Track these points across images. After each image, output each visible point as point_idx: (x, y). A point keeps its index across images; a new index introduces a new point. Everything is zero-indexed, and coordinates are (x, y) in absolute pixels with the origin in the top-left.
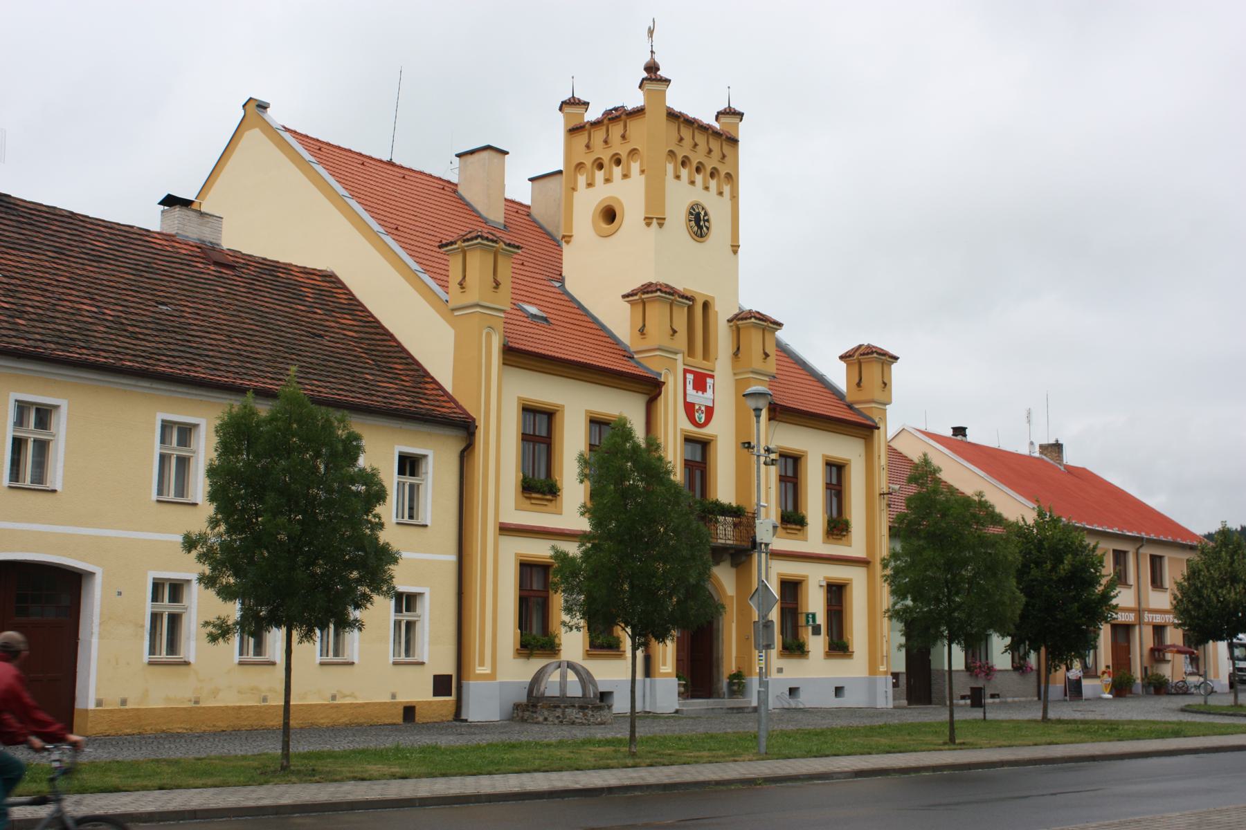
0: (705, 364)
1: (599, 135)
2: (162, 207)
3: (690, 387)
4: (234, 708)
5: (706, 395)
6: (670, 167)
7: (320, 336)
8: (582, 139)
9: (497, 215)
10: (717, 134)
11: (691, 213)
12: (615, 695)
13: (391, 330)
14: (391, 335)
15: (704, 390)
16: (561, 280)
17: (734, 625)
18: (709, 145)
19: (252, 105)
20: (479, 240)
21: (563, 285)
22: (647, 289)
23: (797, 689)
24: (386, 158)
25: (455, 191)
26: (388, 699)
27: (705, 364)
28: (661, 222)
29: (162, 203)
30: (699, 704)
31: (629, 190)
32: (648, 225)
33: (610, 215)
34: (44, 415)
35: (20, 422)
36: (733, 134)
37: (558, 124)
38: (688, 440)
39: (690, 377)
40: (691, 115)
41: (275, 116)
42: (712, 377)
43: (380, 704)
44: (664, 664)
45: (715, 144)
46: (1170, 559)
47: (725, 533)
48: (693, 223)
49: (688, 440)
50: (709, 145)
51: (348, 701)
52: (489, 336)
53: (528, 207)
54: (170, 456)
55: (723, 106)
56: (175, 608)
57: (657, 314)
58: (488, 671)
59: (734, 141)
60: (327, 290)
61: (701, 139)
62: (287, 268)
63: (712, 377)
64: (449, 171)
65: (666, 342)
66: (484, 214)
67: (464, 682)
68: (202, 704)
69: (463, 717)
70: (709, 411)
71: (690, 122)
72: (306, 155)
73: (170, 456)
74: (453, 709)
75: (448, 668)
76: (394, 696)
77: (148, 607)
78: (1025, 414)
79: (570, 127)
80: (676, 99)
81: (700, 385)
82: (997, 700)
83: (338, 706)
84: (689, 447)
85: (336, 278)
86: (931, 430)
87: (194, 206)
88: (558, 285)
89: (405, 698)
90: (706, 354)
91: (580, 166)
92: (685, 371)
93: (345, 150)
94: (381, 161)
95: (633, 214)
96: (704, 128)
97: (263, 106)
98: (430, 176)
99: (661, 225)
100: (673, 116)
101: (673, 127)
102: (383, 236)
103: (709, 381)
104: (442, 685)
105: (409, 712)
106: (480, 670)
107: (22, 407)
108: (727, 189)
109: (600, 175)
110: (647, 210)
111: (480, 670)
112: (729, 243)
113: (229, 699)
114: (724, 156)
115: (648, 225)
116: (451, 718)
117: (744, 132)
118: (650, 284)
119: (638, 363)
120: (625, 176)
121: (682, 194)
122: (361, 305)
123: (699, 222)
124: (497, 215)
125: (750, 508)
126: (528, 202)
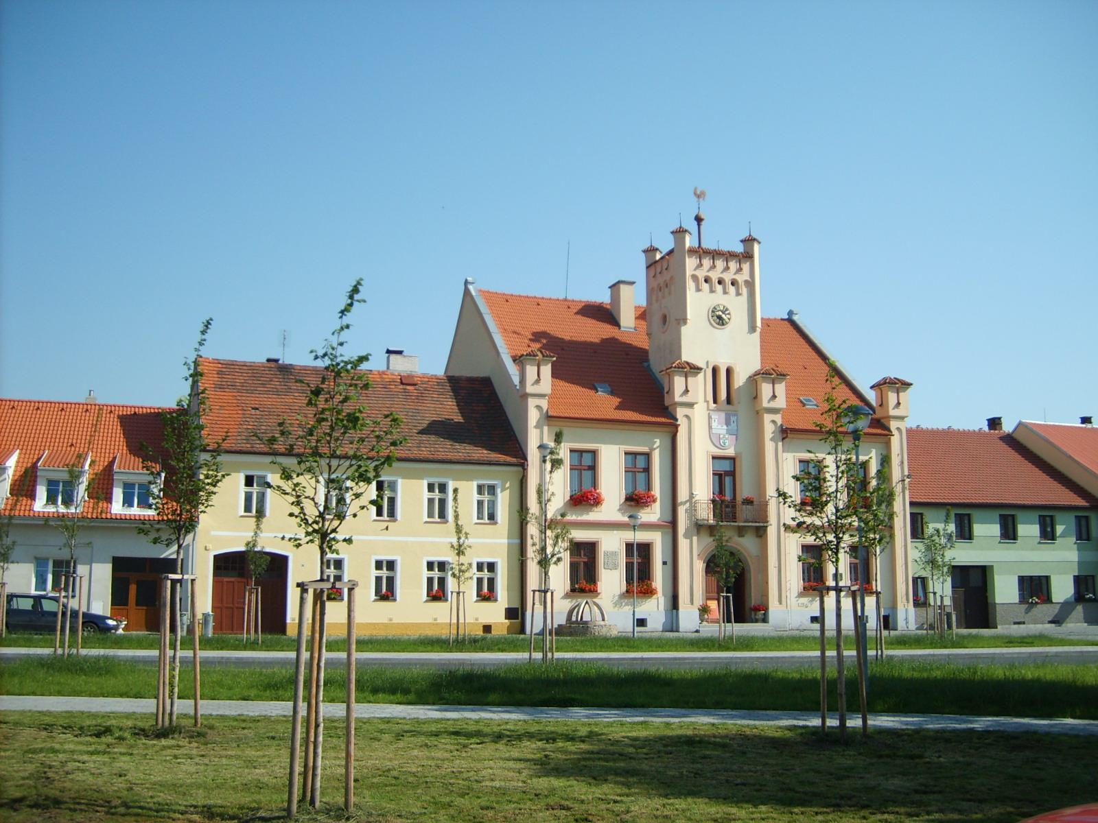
83: (437, 624)
105: (487, 628)
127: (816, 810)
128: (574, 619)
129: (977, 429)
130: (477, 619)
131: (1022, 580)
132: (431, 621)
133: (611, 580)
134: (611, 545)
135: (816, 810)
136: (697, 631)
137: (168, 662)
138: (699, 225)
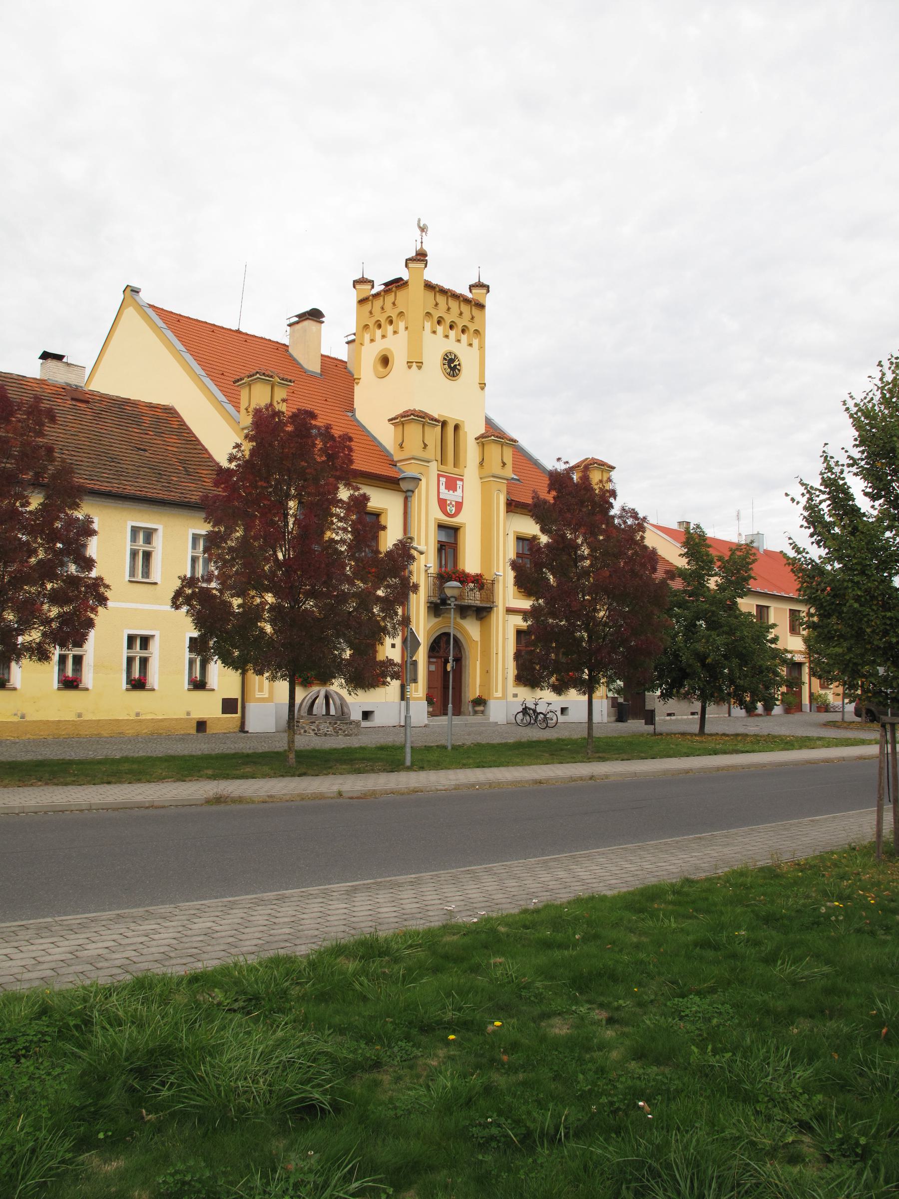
0: (456, 470)
1: (378, 303)
2: (41, 361)
3: (442, 488)
4: (53, 722)
5: (456, 493)
6: (428, 325)
7: (145, 450)
8: (367, 307)
9: (314, 366)
10: (467, 301)
11: (445, 359)
12: (376, 714)
13: (207, 447)
14: (206, 450)
15: (455, 490)
16: (353, 411)
17: (478, 663)
18: (463, 308)
19: (129, 289)
20: (258, 375)
21: (354, 415)
22: (405, 415)
23: (567, 708)
24: (235, 328)
25: (346, 368)
26: (184, 716)
27: (456, 470)
28: (420, 365)
29: (40, 358)
30: (443, 720)
31: (396, 343)
32: (410, 367)
33: (385, 361)
34: (149, 535)
35: (134, 539)
36: (481, 301)
37: (352, 296)
38: (441, 527)
39: (443, 480)
40: (446, 286)
41: (146, 297)
42: (462, 480)
43: (176, 719)
44: (496, 692)
45: (465, 309)
46: (775, 608)
47: (474, 598)
48: (446, 366)
49: (441, 527)
50: (463, 308)
51: (149, 717)
52: (498, 495)
53: (346, 362)
54: (198, 558)
55: (474, 281)
56: (144, 654)
57: (414, 431)
58: (267, 696)
59: (481, 306)
60: (166, 419)
61: (453, 304)
62: (135, 404)
63: (462, 480)
64: (280, 334)
65: (418, 452)
66: (305, 366)
67: (247, 704)
68: (28, 718)
69: (246, 729)
70: (459, 506)
71: (443, 292)
72: (160, 323)
73: (198, 558)
74: (239, 723)
75: (235, 693)
76: (188, 714)
77: (125, 653)
78: (735, 514)
79: (361, 297)
80: (433, 274)
81: (451, 485)
82: (673, 718)
83: (140, 721)
84: (443, 533)
85: (177, 413)
86: (661, 524)
87: (65, 360)
88: (350, 414)
89: (199, 714)
90: (456, 465)
91: (366, 327)
92: (439, 476)
93: (202, 322)
94: (230, 330)
95: (399, 362)
96: (456, 296)
97: (136, 291)
98: (270, 340)
99: (419, 368)
100: (429, 286)
101: (430, 295)
102: (202, 378)
103: (459, 483)
104: (229, 706)
105: (201, 726)
106: (258, 695)
107: (135, 530)
108: (476, 342)
109: (379, 333)
110: (408, 358)
111: (258, 695)
112: (477, 381)
113: (53, 715)
114: (473, 318)
115: (410, 367)
116: (237, 729)
117: (490, 301)
118: (407, 412)
119: (400, 469)
120: (395, 332)
121: (436, 345)
122: (188, 428)
123: (452, 366)
124: (314, 366)
125: (487, 577)
126: (345, 359)
131: (224, 700)
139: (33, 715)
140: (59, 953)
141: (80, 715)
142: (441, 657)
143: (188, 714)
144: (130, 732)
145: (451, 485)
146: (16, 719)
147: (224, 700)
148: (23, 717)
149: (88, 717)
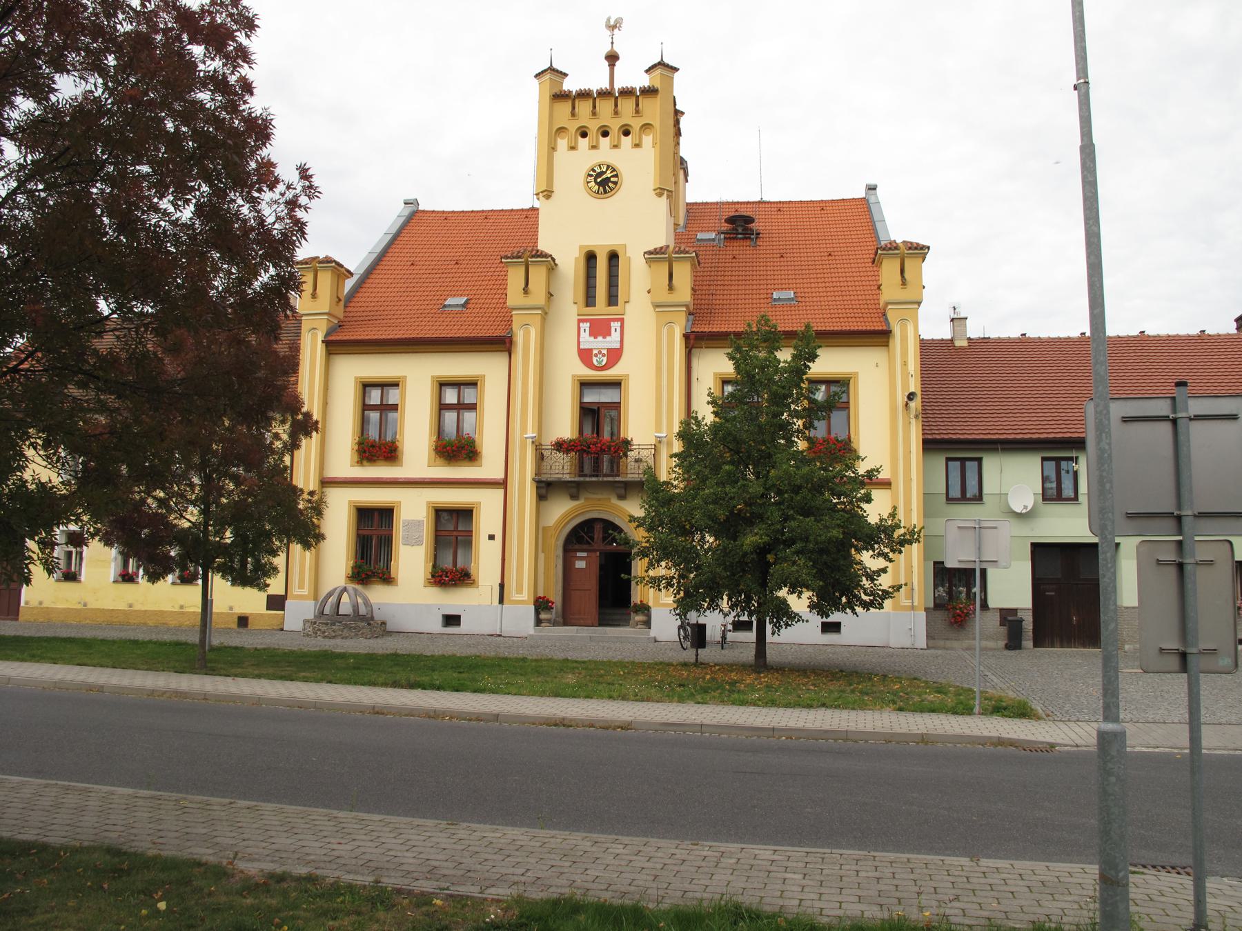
27: (613, 309)
39: (586, 326)
63: (622, 320)
83: (183, 613)
90: (612, 299)
92: (579, 321)
105: (243, 621)
113: (108, 604)
127: (808, 850)
128: (327, 611)
129: (1135, 333)
130: (231, 608)
131: (1033, 545)
132: (177, 609)
133: (411, 559)
134: (413, 510)
135: (808, 850)
136: (984, 606)
137: (170, 598)
138: (612, 65)
139: (93, 604)
140: (39, 672)
141: (131, 606)
142: (595, 551)
143: (231, 608)
144: (173, 623)
145: (600, 328)
146: (80, 607)
147: (1033, 545)
148: (85, 605)
149: (137, 607)
